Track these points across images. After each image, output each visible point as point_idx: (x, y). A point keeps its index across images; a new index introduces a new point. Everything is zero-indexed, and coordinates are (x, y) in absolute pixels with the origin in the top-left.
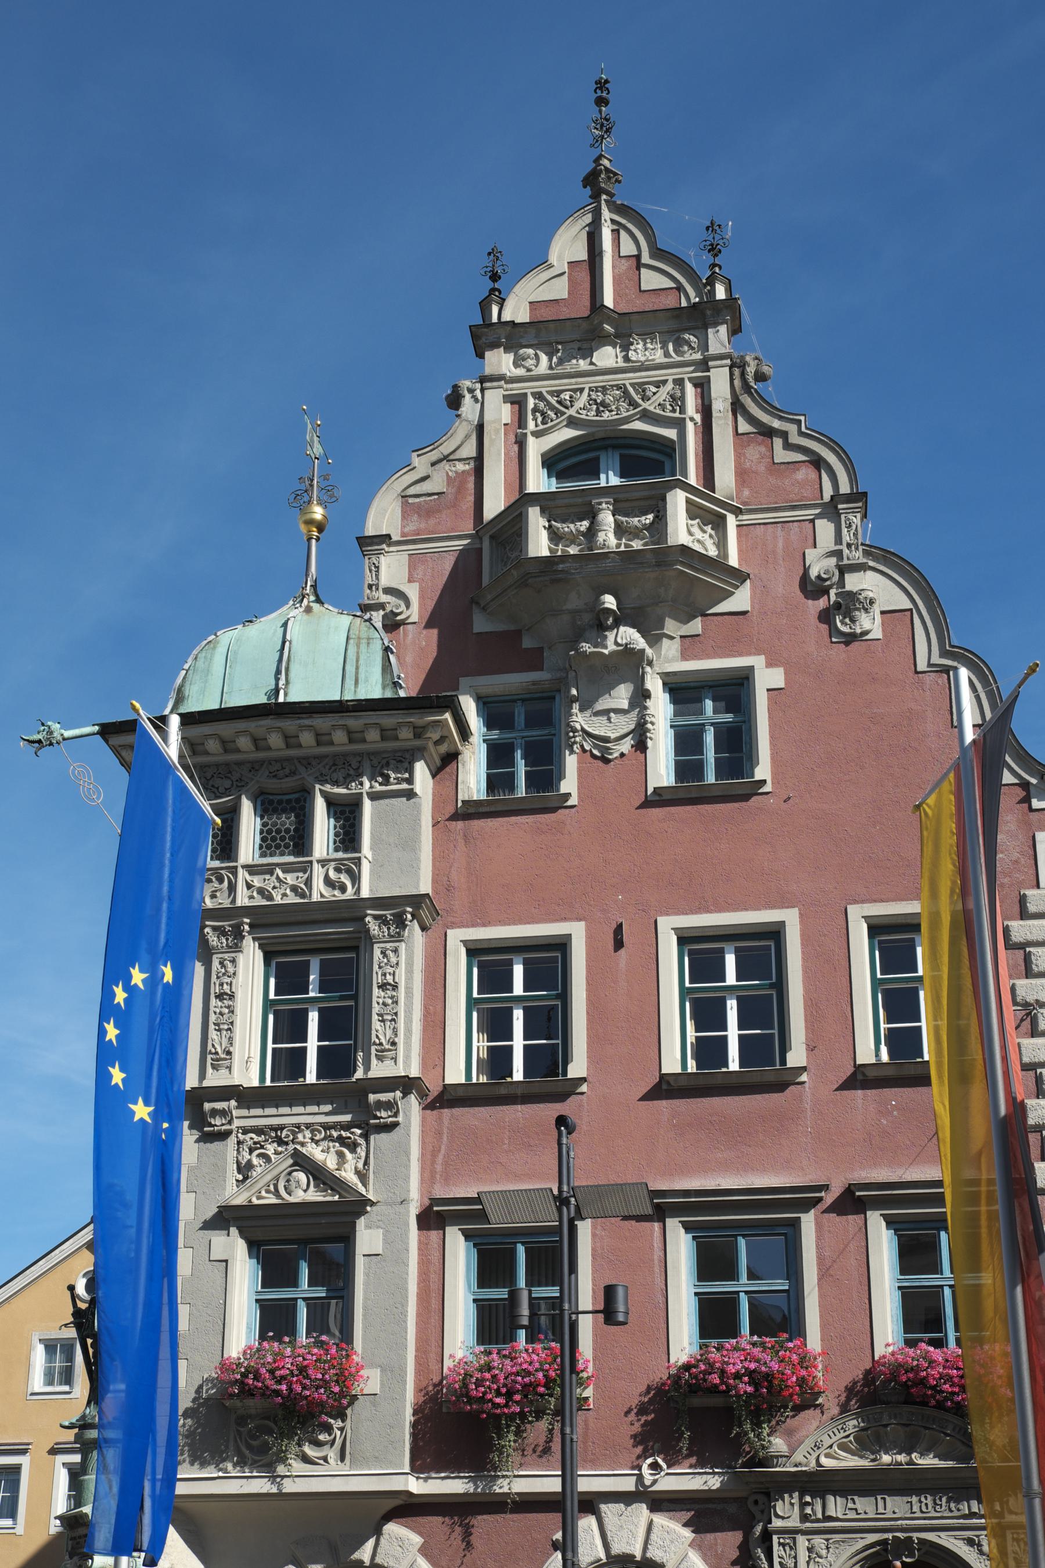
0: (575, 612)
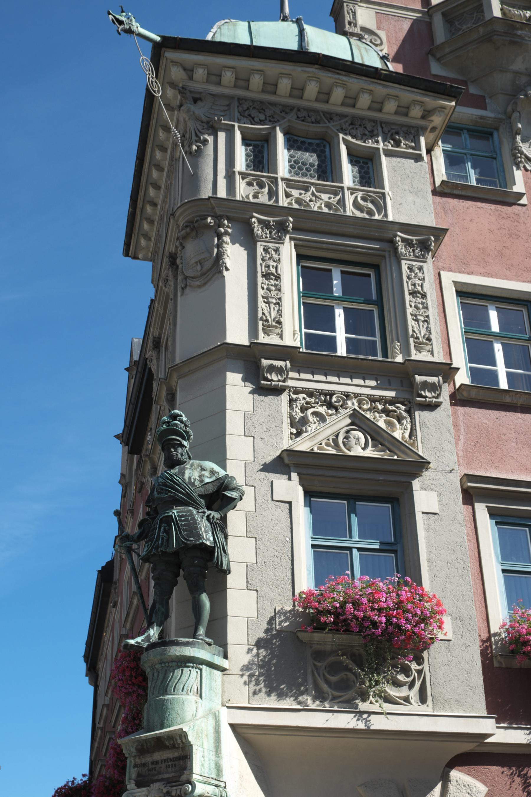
0: (517, 73)
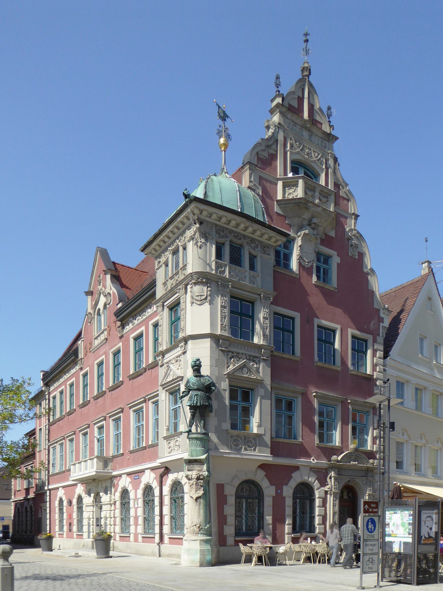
0: (304, 219)
